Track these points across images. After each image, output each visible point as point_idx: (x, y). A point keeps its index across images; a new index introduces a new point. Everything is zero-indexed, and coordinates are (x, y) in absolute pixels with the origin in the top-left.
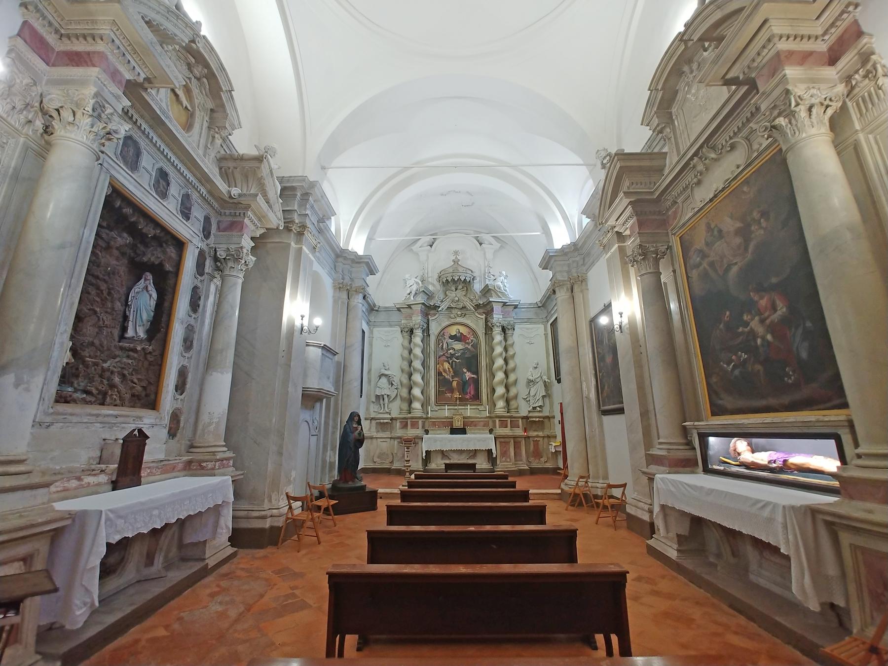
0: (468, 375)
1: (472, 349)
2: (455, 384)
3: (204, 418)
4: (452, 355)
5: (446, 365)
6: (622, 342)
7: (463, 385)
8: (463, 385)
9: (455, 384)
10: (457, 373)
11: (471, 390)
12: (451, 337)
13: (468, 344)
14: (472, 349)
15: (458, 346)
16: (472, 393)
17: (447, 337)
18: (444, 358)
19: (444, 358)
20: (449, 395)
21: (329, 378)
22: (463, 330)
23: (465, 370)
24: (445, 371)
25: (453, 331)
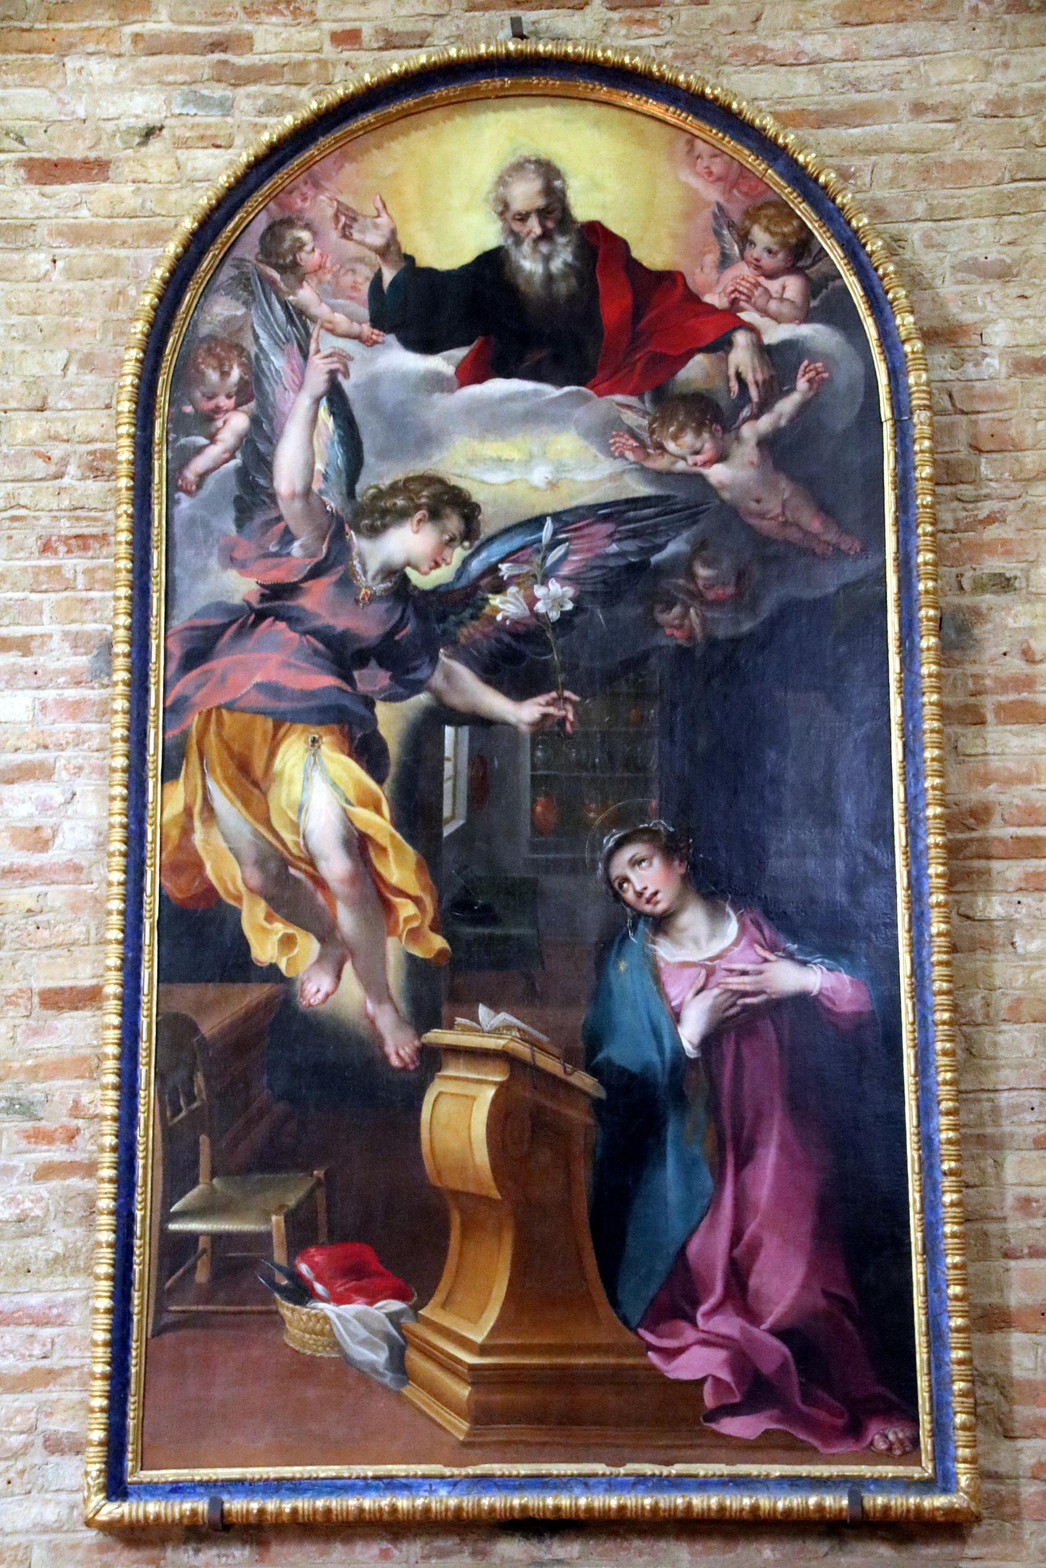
0: (702, 966)
1: (777, 504)
2: (459, 1120)
3: (473, 1134)
4: (425, 621)
5: (320, 792)
6: (997, 1337)
7: (611, 1140)
8: (611, 1140)
9: (459, 1120)
10: (500, 921)
11: (748, 1226)
12: (422, 306)
13: (712, 414)
14: (777, 504)
15: (537, 454)
16: (783, 1282)
17: (335, 305)
18: (274, 661)
19: (274, 661)
20: (353, 1324)
21: (766, 960)
22: (619, 176)
23: (647, 876)
24: (290, 886)
25: (451, 193)
